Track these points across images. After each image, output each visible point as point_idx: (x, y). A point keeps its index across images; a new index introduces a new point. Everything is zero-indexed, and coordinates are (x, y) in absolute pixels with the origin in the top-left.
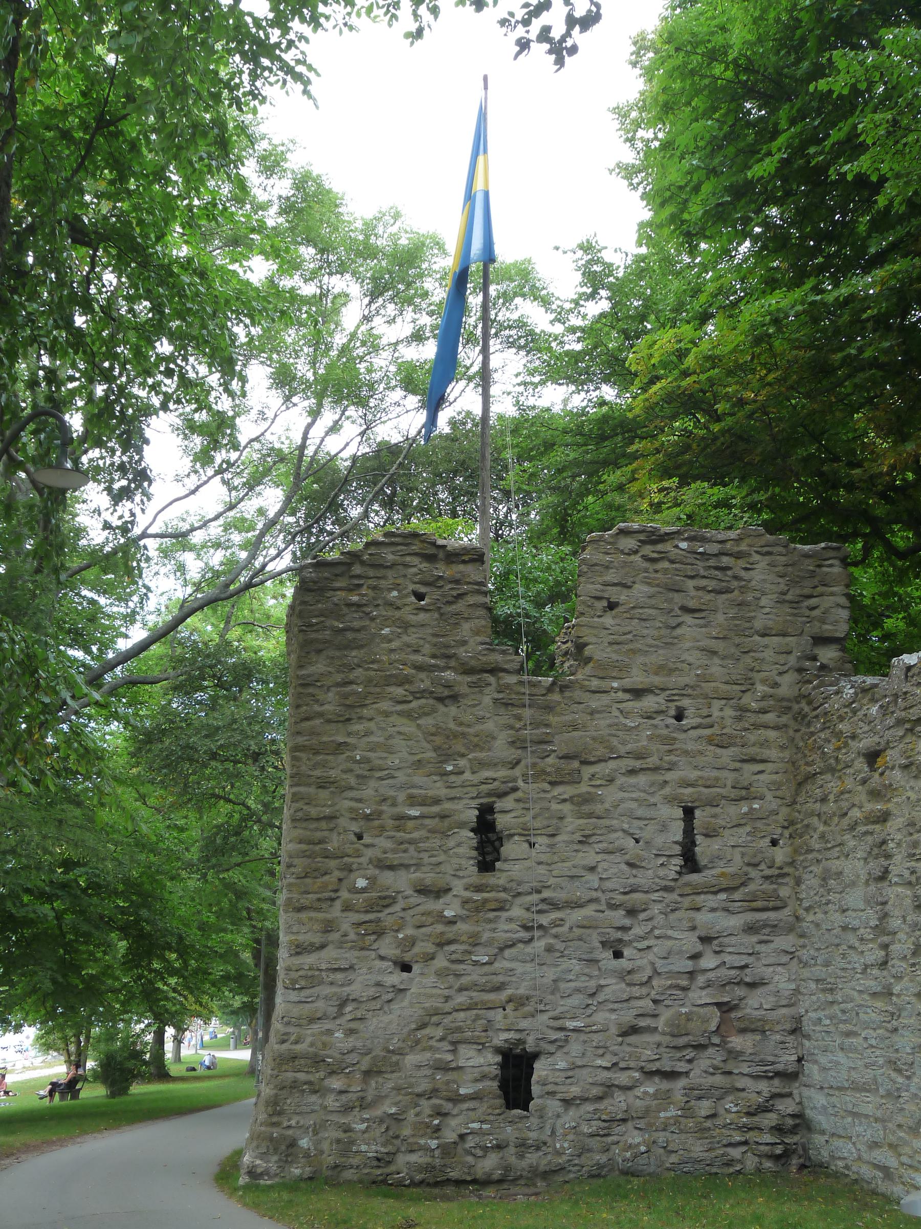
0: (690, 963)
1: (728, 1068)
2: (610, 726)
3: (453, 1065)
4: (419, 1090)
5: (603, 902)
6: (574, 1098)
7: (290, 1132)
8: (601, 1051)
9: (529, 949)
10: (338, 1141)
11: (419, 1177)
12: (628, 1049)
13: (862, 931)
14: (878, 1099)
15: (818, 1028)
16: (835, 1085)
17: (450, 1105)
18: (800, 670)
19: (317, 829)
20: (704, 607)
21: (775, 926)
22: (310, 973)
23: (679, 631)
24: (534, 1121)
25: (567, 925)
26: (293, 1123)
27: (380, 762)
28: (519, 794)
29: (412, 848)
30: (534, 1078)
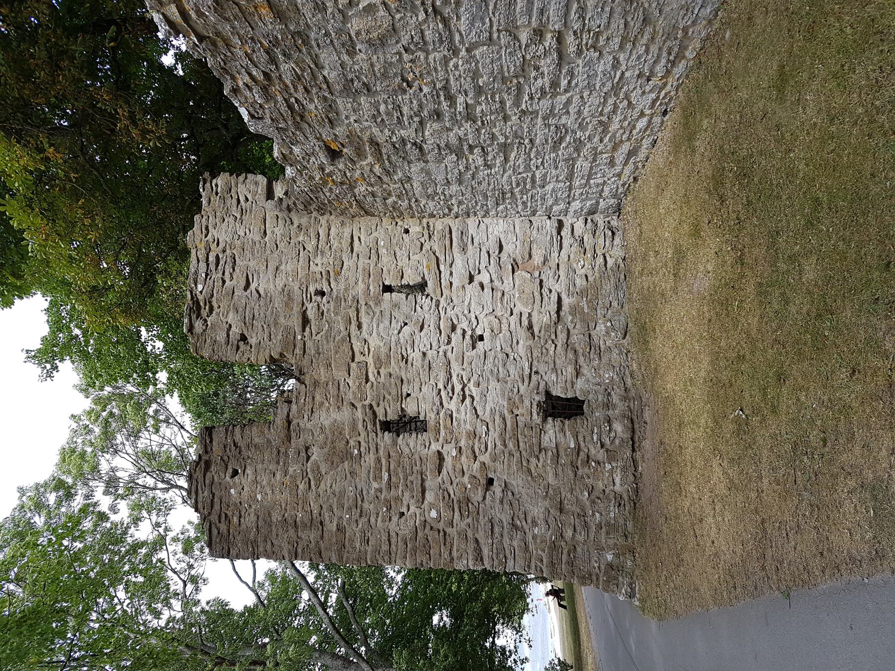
0: (486, 290)
1: (554, 267)
2: (328, 342)
3: (555, 451)
4: (572, 475)
5: (446, 347)
6: (576, 369)
7: (603, 567)
8: (544, 351)
9: (477, 398)
10: (608, 533)
11: (632, 478)
12: (543, 332)
13: (461, 167)
14: (580, 159)
15: (529, 204)
16: (567, 193)
17: (581, 453)
18: (289, 209)
19: (397, 546)
20: (245, 275)
21: (462, 233)
22: (495, 551)
23: (262, 292)
24: (591, 397)
25: (461, 372)
26: (596, 565)
27: (351, 501)
28: (374, 404)
29: (410, 478)
30: (563, 396)
